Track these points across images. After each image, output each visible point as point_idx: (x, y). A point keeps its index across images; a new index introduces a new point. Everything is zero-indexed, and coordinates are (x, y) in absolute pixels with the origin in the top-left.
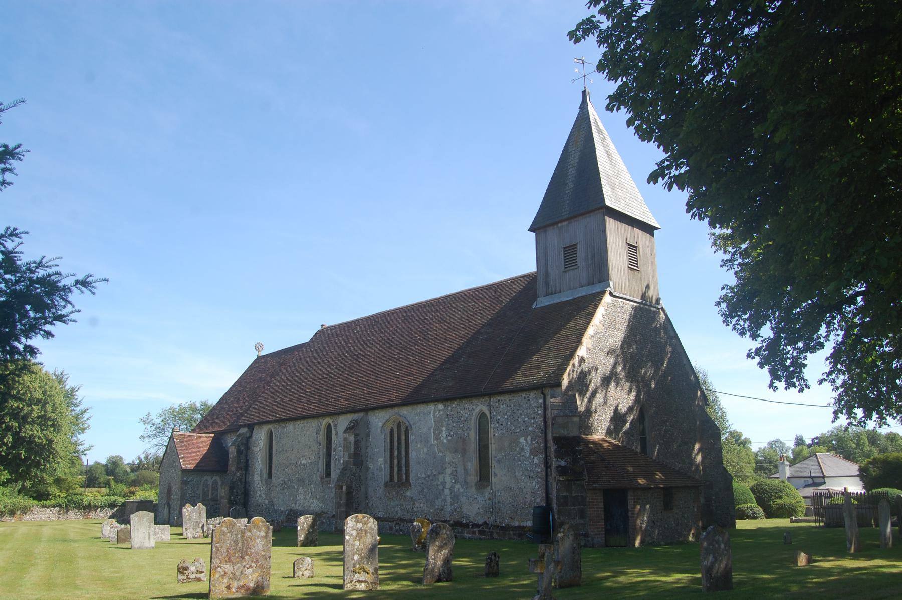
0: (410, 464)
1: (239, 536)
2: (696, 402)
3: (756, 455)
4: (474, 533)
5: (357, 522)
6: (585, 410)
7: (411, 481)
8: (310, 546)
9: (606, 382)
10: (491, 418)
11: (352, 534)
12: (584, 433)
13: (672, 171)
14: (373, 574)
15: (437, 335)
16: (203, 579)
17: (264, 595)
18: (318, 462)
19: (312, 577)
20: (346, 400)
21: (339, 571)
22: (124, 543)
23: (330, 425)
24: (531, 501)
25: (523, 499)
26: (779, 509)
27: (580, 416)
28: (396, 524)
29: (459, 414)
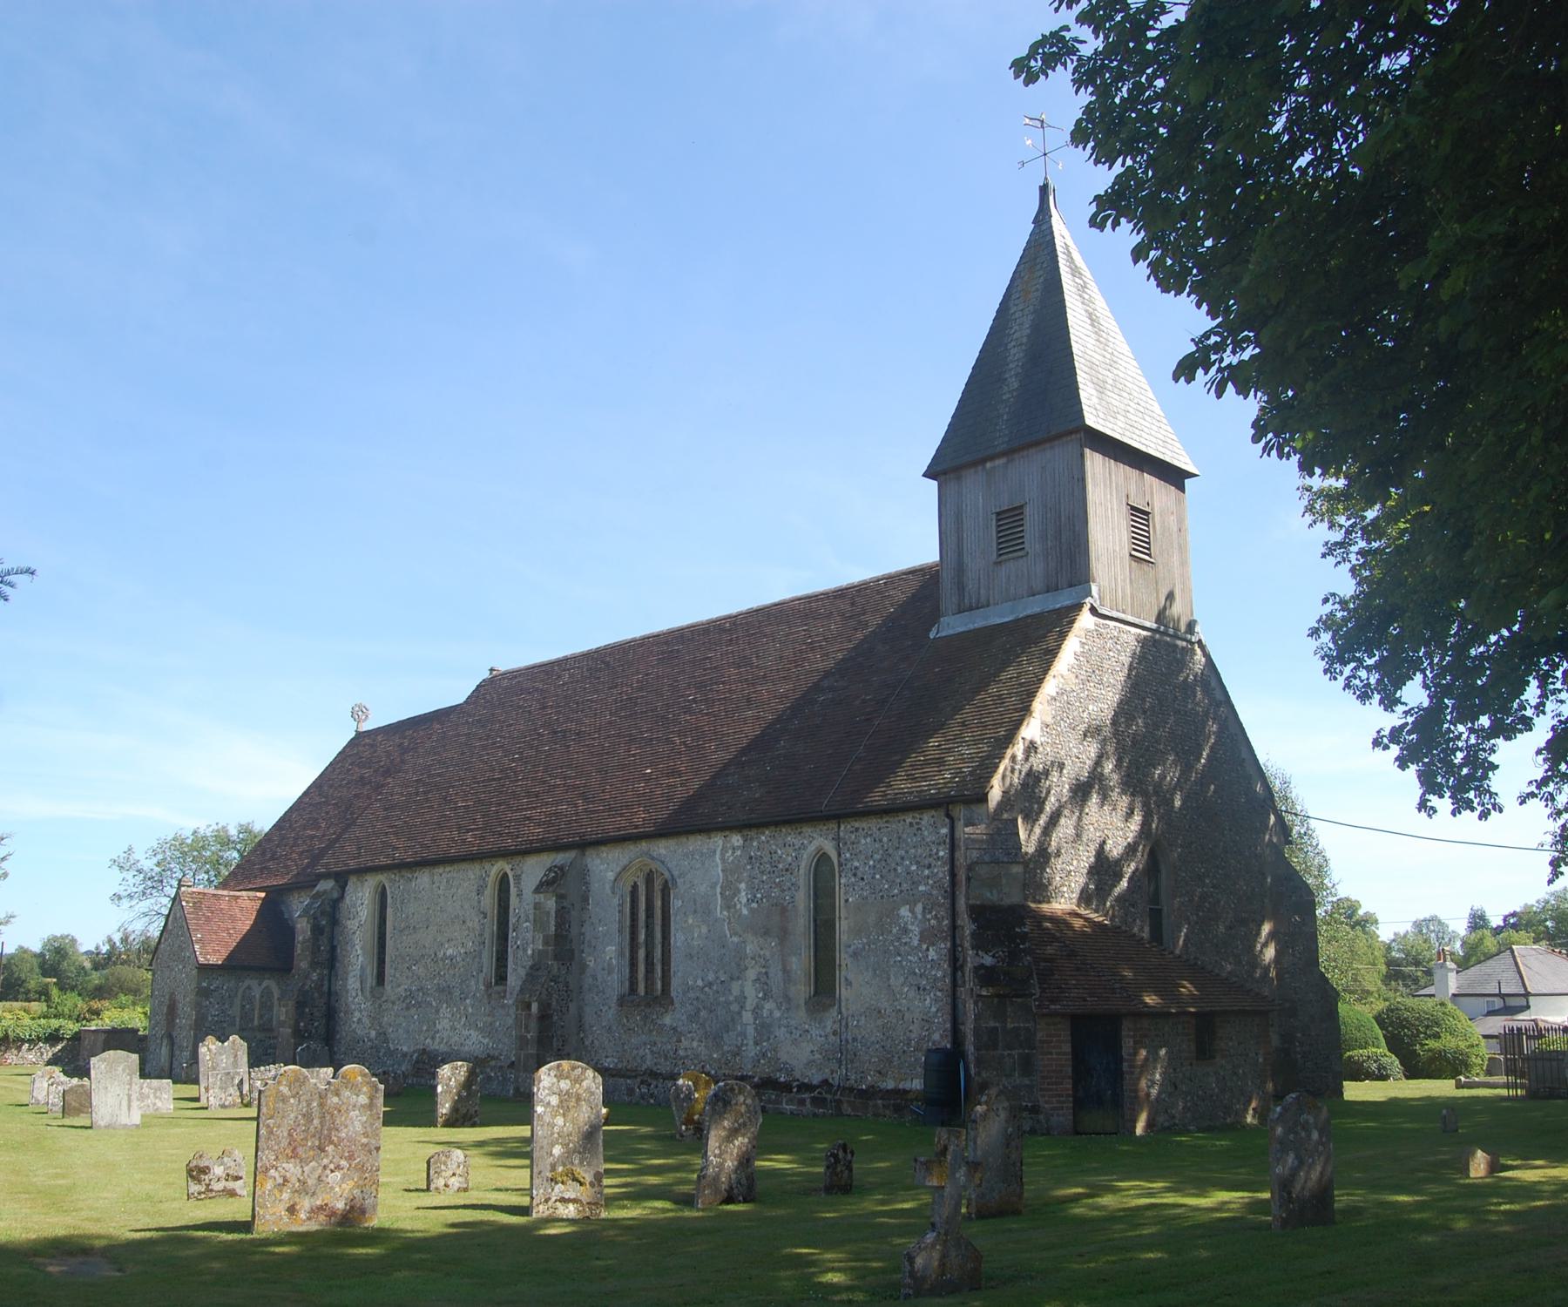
0: (672, 959)
2: (1267, 837)
3: (1389, 948)
4: (802, 1102)
5: (560, 1077)
6: (1036, 850)
7: (673, 994)
8: (463, 1125)
10: (840, 865)
11: (549, 1103)
12: (1034, 897)
13: (1225, 356)
14: (592, 1184)
15: (730, 691)
17: (366, 1225)
18: (480, 953)
19: (466, 1190)
20: (539, 825)
21: (520, 1177)
22: (78, 1115)
23: (505, 875)
24: (921, 1039)
25: (905, 1034)
26: (1432, 1060)
27: (1026, 864)
28: (642, 1082)
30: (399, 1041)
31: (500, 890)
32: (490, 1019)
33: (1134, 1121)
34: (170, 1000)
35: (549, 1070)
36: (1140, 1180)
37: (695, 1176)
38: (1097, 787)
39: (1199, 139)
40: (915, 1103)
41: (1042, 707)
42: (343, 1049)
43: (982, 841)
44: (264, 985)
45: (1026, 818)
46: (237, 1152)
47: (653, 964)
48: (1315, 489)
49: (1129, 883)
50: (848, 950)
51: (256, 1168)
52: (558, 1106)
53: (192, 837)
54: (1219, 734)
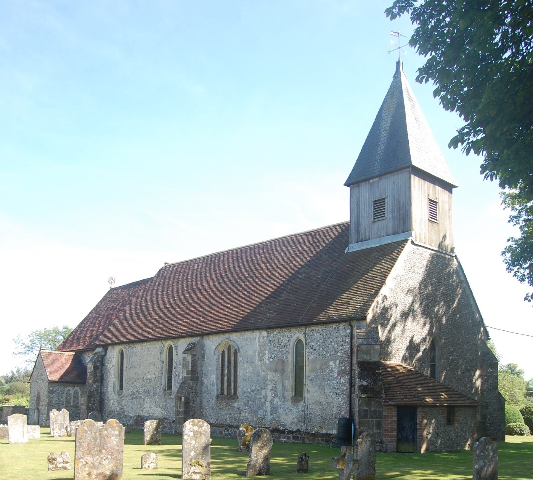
0: (238, 381)
1: (98, 434)
2: (480, 337)
3: (528, 384)
4: (289, 438)
5: (194, 425)
6: (385, 340)
7: (238, 395)
8: (155, 444)
10: (306, 344)
12: (384, 359)
13: (470, 137)
14: (206, 467)
15: (263, 273)
16: (68, 468)
20: (185, 326)
21: (178, 464)
22: (3, 439)
23: (171, 346)
28: (226, 429)
29: (280, 341)
30: (129, 411)
31: (169, 352)
32: (165, 403)
33: (421, 448)
34: (38, 394)
36: (420, 470)
37: (246, 465)
38: (411, 315)
39: (463, 44)
40: (334, 439)
41: (390, 281)
42: (107, 415)
43: (364, 336)
44: (75, 389)
45: (382, 326)
47: (230, 382)
48: (507, 194)
49: (422, 353)
50: (309, 378)
51: (75, 458)
52: (193, 436)
53: (44, 331)
54: (462, 294)
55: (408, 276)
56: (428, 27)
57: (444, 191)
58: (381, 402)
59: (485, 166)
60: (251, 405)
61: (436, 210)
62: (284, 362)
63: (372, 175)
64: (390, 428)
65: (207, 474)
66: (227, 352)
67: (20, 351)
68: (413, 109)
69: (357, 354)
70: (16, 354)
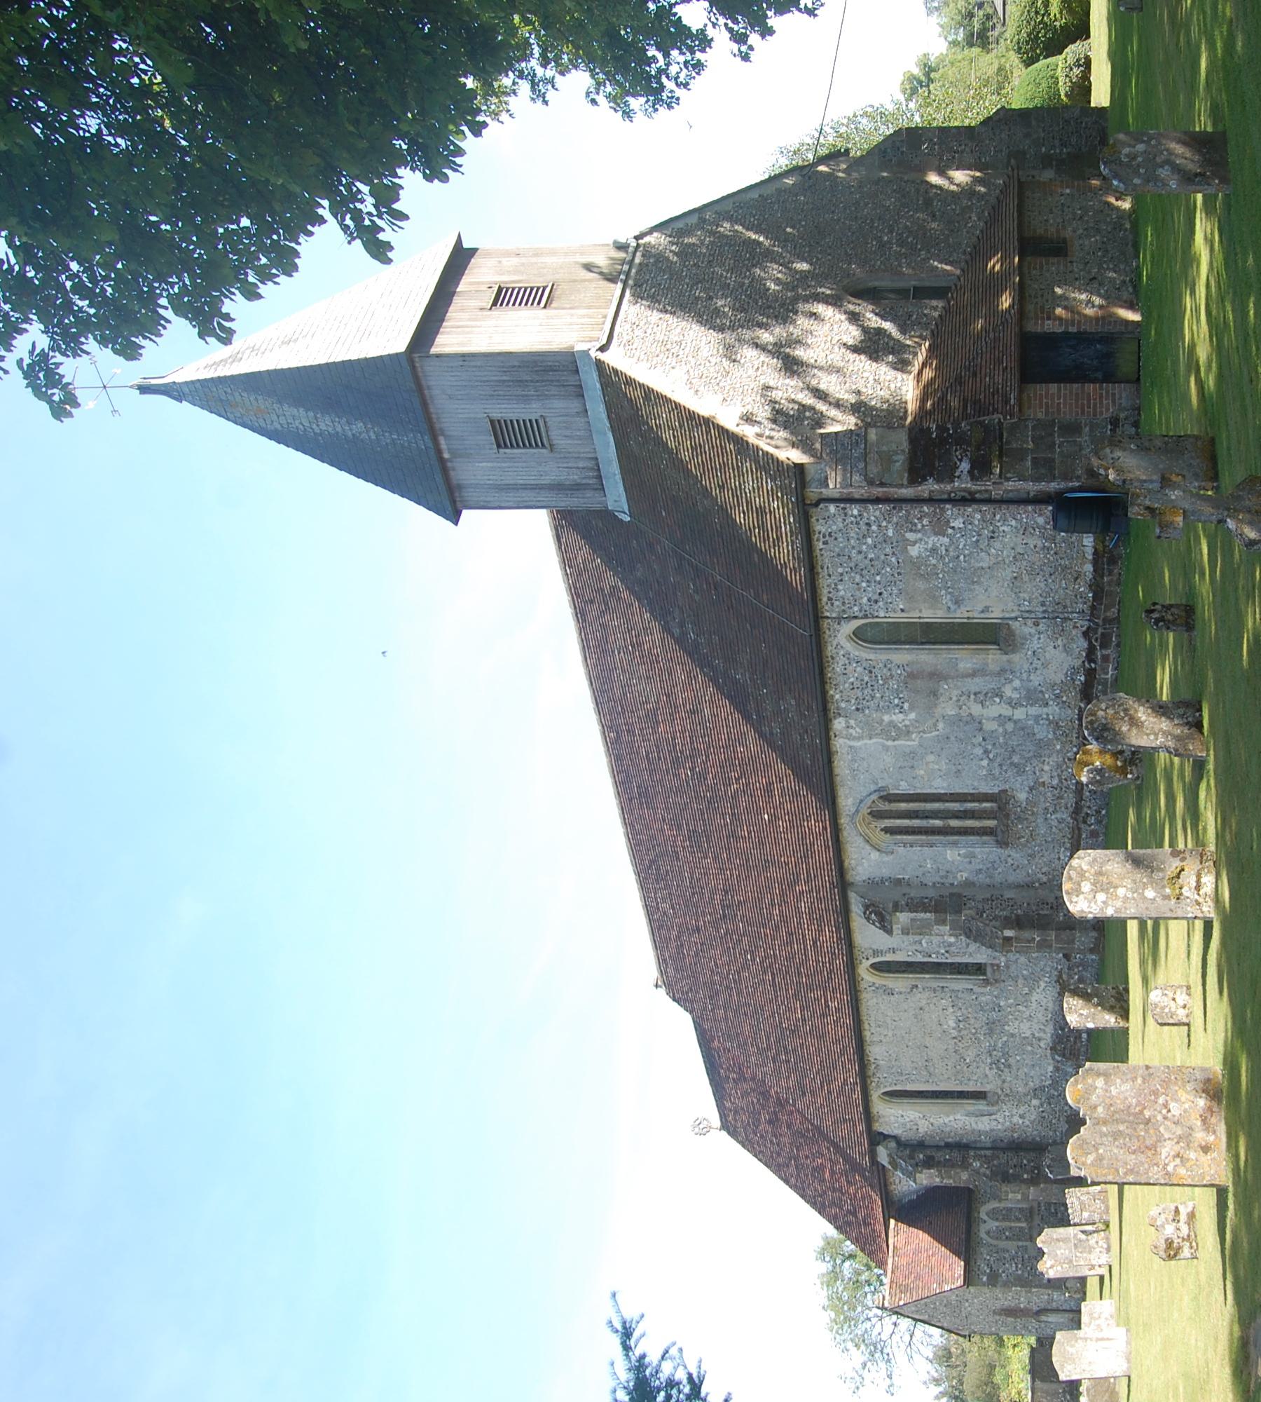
0: (961, 791)
1: (1105, 1129)
2: (841, 174)
3: (954, 43)
4: (1106, 659)
5: (1078, 892)
6: (853, 414)
7: (996, 790)
8: (1127, 1001)
9: (795, 368)
10: (866, 617)
11: (1104, 903)
12: (901, 418)
13: (365, 211)
14: (1183, 859)
15: (683, 732)
16: (1190, 1209)
17: (1220, 1077)
19: (1188, 988)
20: (821, 931)
21: (1176, 930)
22: (1117, 1393)
23: (874, 966)
24: (1043, 536)
25: (1037, 552)
26: (1071, 11)
27: (867, 425)
28: (1085, 822)
29: (857, 684)
30: (1042, 1075)
31: (889, 971)
32: (1020, 981)
33: (1127, 323)
35: (1071, 902)
37: (1176, 760)
38: (788, 350)
41: (704, 405)
42: (1051, 1133)
43: (844, 470)
46: (1151, 1213)
47: (965, 811)
51: (1166, 1184)
52: (1107, 893)
55: (690, 358)
56: (94, 316)
57: (471, 269)
58: (1012, 424)
59: (428, 172)
60: (1022, 757)
61: (520, 289)
62: (912, 672)
63: (432, 453)
64: (1077, 401)
65: (1202, 857)
66: (886, 821)
67: (883, 1373)
68: (262, 349)
69: (891, 485)
70: (891, 1385)
